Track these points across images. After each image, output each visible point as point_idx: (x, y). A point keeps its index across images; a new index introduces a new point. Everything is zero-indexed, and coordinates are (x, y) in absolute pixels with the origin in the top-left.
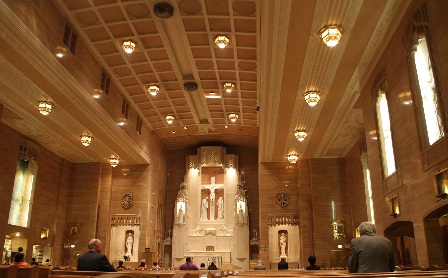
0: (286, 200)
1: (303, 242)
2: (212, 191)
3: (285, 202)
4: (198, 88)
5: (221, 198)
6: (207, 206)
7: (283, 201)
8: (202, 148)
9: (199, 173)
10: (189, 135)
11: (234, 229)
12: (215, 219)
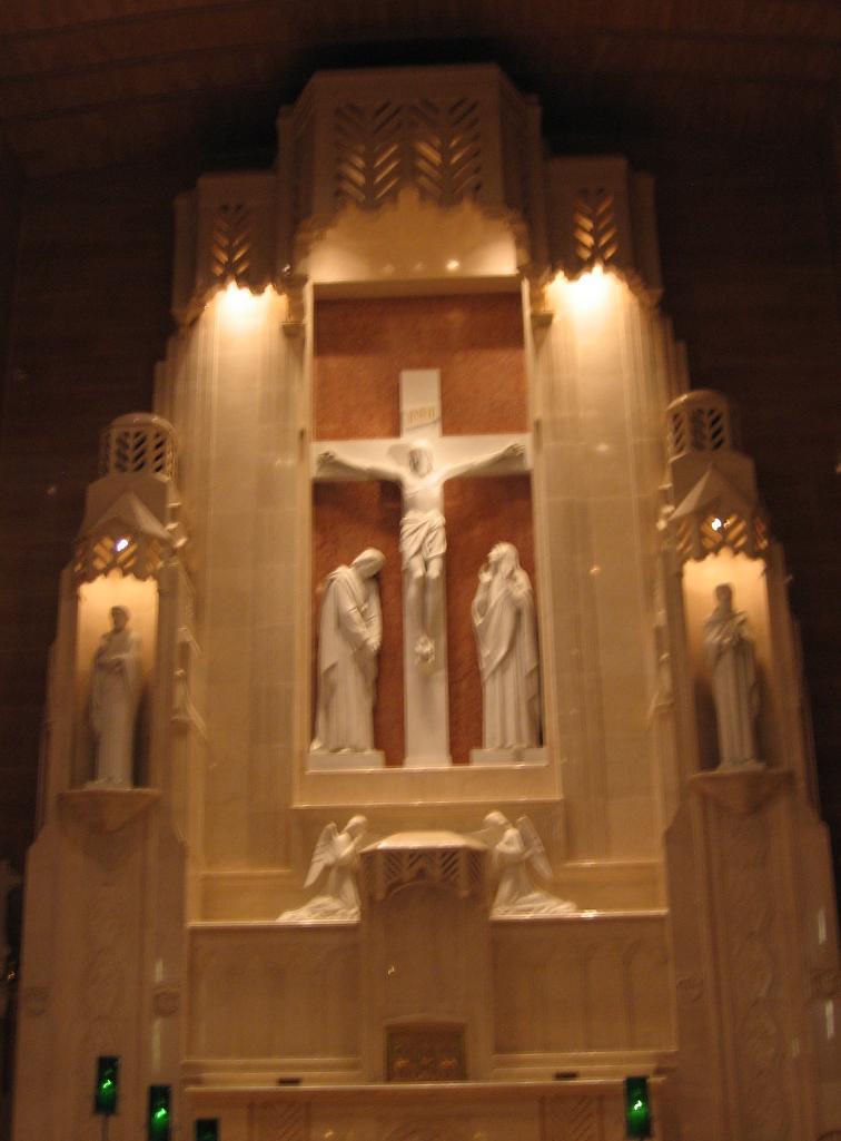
2: (426, 491)
5: (503, 551)
6: (372, 636)
8: (327, 87)
9: (291, 332)
11: (670, 837)
12: (459, 753)
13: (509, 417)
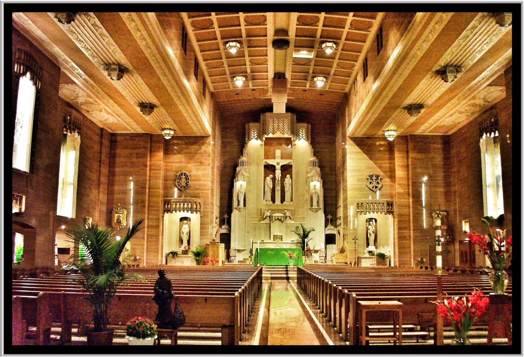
0: (378, 183)
1: (399, 233)
2: (278, 167)
3: (377, 185)
4: (290, 45)
5: (288, 176)
7: (375, 184)
10: (255, 98)
12: (282, 202)
13: (290, 157)
